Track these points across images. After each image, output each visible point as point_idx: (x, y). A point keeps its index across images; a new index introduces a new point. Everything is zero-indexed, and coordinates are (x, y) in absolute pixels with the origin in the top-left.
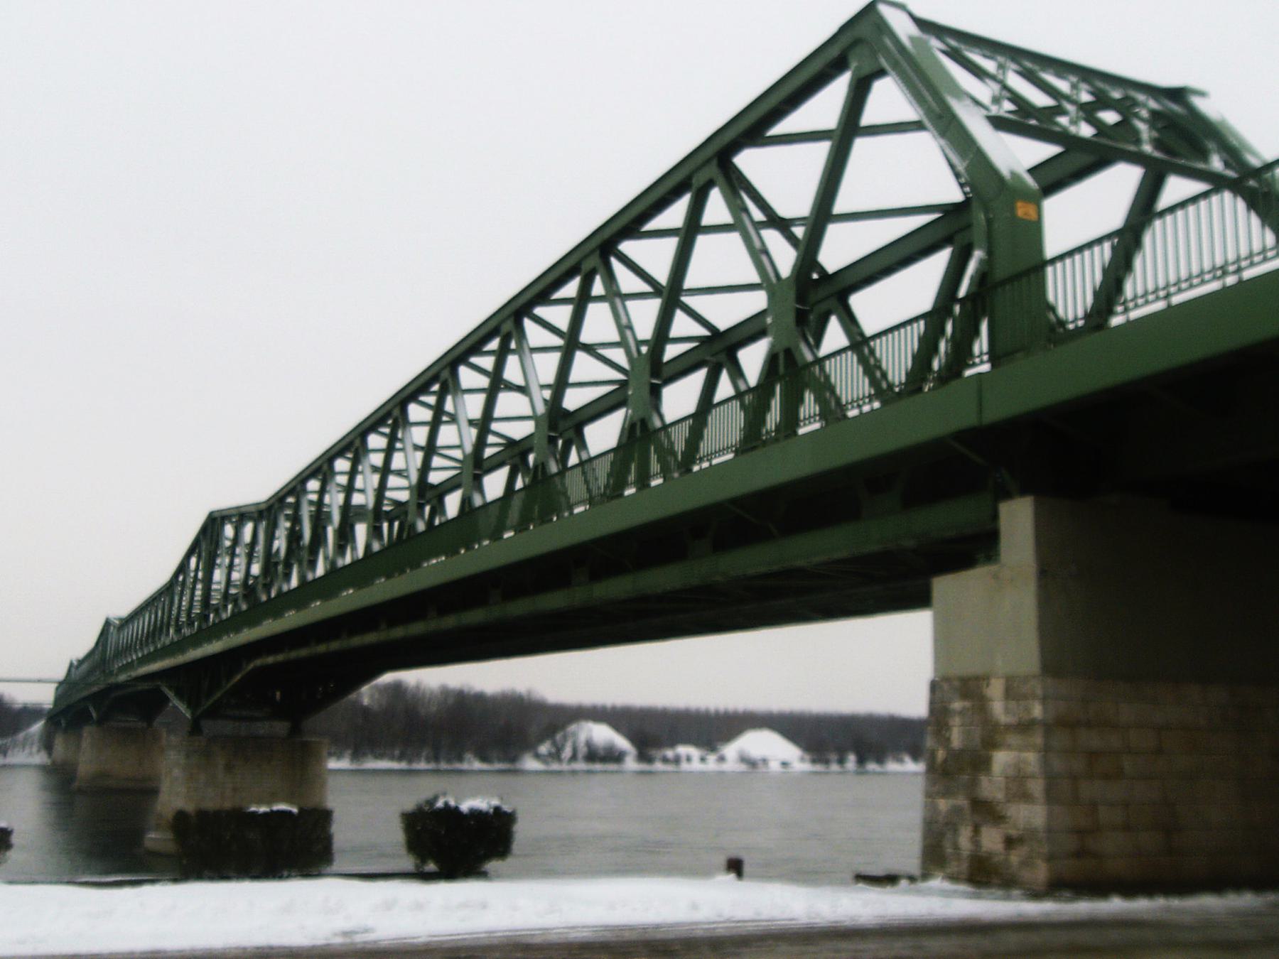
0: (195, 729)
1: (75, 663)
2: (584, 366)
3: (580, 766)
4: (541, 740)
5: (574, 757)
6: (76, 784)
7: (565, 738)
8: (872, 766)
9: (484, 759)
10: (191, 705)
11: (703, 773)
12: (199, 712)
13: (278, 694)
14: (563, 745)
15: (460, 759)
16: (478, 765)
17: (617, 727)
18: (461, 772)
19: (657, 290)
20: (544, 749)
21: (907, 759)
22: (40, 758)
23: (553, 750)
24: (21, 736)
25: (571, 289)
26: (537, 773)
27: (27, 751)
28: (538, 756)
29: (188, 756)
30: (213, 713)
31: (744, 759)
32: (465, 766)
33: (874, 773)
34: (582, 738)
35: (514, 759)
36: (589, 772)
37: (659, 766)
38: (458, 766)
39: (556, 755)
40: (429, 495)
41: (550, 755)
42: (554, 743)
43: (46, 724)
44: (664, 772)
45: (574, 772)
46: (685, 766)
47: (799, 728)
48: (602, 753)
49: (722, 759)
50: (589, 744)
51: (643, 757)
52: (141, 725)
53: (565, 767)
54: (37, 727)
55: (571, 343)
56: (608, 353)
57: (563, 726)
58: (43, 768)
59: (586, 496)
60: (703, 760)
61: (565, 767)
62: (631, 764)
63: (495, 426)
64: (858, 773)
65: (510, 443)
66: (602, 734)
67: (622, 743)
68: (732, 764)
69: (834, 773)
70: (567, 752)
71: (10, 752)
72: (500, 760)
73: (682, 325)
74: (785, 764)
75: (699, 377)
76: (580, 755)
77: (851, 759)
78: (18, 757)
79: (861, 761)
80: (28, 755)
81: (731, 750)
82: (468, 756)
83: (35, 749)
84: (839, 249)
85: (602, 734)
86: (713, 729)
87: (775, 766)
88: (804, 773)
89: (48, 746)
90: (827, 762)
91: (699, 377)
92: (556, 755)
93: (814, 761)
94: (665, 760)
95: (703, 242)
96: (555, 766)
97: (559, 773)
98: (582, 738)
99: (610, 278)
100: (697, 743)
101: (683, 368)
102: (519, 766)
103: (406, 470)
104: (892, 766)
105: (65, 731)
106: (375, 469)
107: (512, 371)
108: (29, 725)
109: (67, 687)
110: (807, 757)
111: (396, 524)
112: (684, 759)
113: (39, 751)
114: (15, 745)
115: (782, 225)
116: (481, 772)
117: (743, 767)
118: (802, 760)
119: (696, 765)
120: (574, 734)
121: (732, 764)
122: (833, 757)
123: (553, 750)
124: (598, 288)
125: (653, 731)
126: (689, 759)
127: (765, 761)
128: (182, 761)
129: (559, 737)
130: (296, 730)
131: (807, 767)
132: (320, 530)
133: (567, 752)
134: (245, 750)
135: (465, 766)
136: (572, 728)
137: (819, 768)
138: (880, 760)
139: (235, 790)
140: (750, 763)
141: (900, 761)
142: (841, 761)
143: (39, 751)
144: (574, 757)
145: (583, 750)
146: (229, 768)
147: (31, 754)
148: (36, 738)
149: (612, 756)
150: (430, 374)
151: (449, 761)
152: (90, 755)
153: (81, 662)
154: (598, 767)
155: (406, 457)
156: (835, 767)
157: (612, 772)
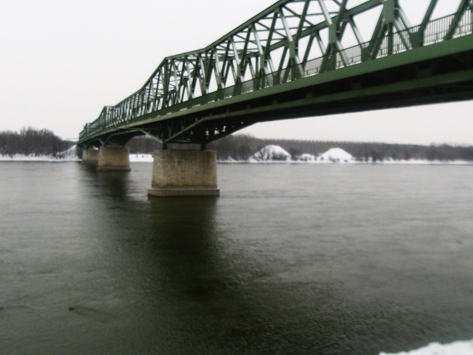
0: (165, 147)
1: (89, 124)
2: (275, 36)
3: (270, 161)
4: (256, 151)
5: (268, 158)
6: (98, 168)
7: (265, 151)
8: (378, 162)
9: (235, 159)
10: (104, 142)
12: (167, 140)
13: (207, 132)
14: (264, 154)
15: (227, 159)
16: (233, 161)
17: (285, 148)
20: (257, 155)
22: (76, 159)
23: (260, 155)
24: (68, 151)
27: (71, 156)
28: (255, 158)
29: (163, 158)
30: (173, 141)
31: (331, 159)
32: (228, 161)
34: (271, 151)
35: (246, 159)
37: (299, 161)
38: (226, 161)
39: (261, 157)
40: (246, 56)
42: (261, 153)
44: (301, 164)
45: (268, 164)
46: (309, 161)
47: (351, 148)
48: (278, 157)
49: (322, 159)
50: (274, 153)
51: (293, 158)
53: (265, 162)
54: (74, 147)
55: (272, 30)
56: (291, 14)
57: (264, 147)
58: (79, 162)
59: (356, 43)
61: (265, 162)
62: (289, 160)
63: (307, 18)
65: (312, 26)
66: (278, 150)
67: (286, 153)
68: (326, 161)
70: (265, 156)
71: (65, 157)
72: (241, 159)
74: (346, 161)
76: (270, 157)
77: (371, 159)
78: (68, 158)
79: (374, 160)
82: (230, 158)
83: (74, 155)
85: (278, 150)
86: (318, 148)
87: (342, 162)
88: (353, 164)
89: (80, 154)
90: (361, 160)
92: (261, 157)
93: (357, 160)
94: (302, 159)
102: (248, 161)
103: (256, 40)
104: (385, 162)
105: (87, 149)
109: (83, 134)
110: (354, 158)
112: (308, 158)
114: (67, 154)
116: (235, 163)
117: (330, 162)
118: (352, 159)
119: (313, 161)
120: (268, 150)
121: (326, 161)
122: (364, 158)
123: (260, 155)
125: (296, 149)
127: (338, 160)
128: (161, 160)
129: (262, 150)
130: (203, 148)
131: (354, 162)
132: (197, 71)
133: (265, 156)
134: (185, 156)
135: (228, 161)
136: (267, 147)
137: (358, 162)
138: (381, 159)
139: (182, 171)
140: (333, 160)
141: (388, 160)
142: (367, 160)
144: (268, 158)
145: (271, 156)
146: (179, 163)
148: (74, 152)
149: (282, 158)
151: (222, 160)
153: (91, 124)
154: (277, 162)
156: (364, 162)
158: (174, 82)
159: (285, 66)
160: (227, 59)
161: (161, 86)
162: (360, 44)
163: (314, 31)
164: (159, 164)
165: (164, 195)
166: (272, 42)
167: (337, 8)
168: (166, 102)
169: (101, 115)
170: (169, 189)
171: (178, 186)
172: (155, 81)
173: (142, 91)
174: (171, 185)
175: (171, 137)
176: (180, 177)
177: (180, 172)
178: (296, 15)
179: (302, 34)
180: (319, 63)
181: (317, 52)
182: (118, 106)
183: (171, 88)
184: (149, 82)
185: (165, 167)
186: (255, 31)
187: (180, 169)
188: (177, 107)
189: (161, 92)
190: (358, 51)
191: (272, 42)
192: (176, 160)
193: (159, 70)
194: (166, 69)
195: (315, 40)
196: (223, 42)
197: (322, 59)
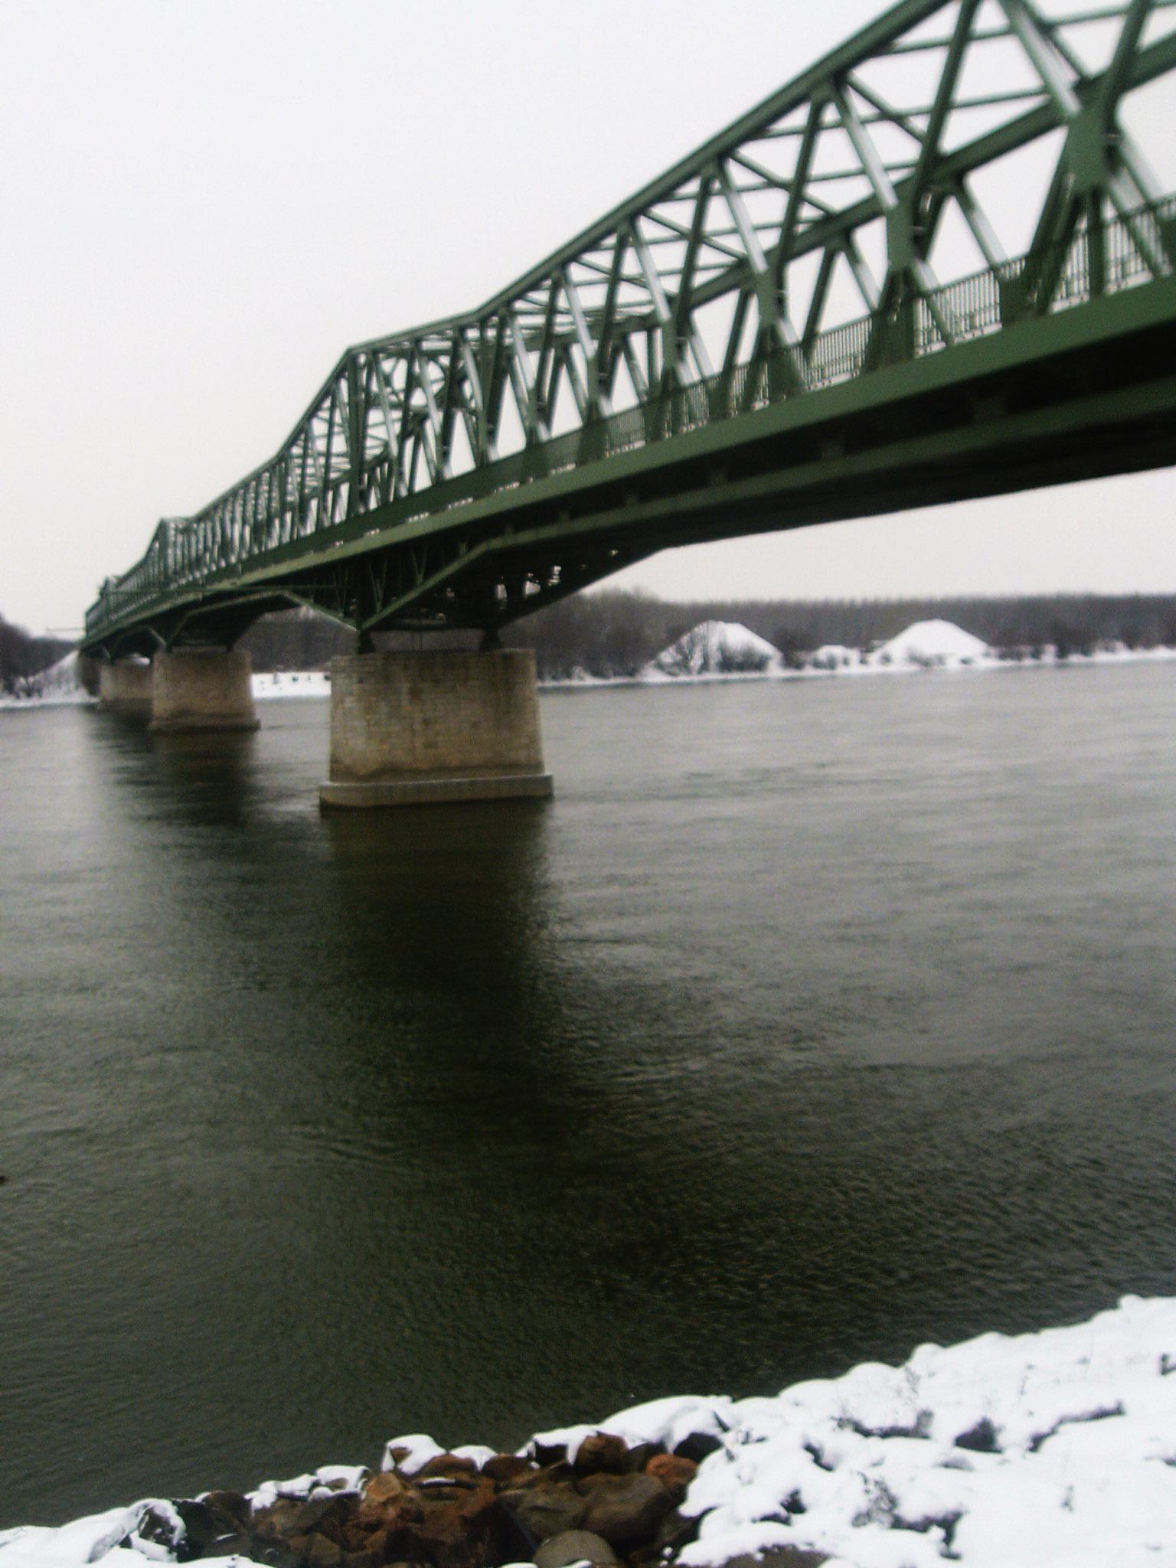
3: (713, 676)
4: (663, 647)
5: (705, 667)
7: (693, 643)
8: (1075, 658)
9: (597, 673)
11: (864, 679)
12: (371, 621)
14: (691, 650)
16: (590, 681)
18: (569, 691)
19: (682, 235)
20: (668, 656)
21: (1119, 645)
22: (81, 696)
23: (679, 657)
24: (54, 671)
25: (799, 117)
26: (663, 686)
27: (64, 688)
28: (661, 667)
29: (361, 681)
31: (914, 659)
32: (575, 683)
33: (1079, 666)
34: (714, 642)
36: (725, 682)
37: (809, 672)
38: (566, 683)
39: (683, 665)
41: (676, 664)
42: (680, 650)
43: (80, 656)
46: (841, 670)
47: (971, 615)
48: (739, 659)
49: (886, 659)
50: (723, 649)
51: (790, 662)
52: (222, 649)
53: (695, 678)
54: (70, 660)
55: (696, 237)
57: (689, 628)
58: (90, 708)
60: (863, 662)
61: (695, 678)
62: (776, 670)
64: (1060, 667)
66: (737, 636)
67: (763, 647)
69: (1027, 668)
70: (696, 661)
71: (45, 691)
72: (616, 674)
73: (807, 212)
75: (731, 300)
78: (55, 696)
79: (1062, 653)
80: (63, 691)
81: (898, 647)
82: (578, 670)
83: (72, 685)
84: (958, 133)
85: (737, 636)
86: (869, 624)
87: (953, 665)
89: (89, 681)
90: (1019, 656)
91: (731, 300)
92: (683, 665)
93: (1002, 657)
94: (817, 665)
95: (975, 54)
96: (683, 678)
97: (689, 685)
98: (714, 642)
99: (844, 108)
100: (848, 643)
101: (713, 292)
102: (638, 679)
104: (1101, 657)
106: (298, 457)
107: (630, 265)
108: (61, 656)
110: (993, 651)
111: (386, 466)
113: (77, 687)
115: (899, 120)
116: (594, 688)
117: (914, 668)
118: (987, 655)
119: (855, 669)
120: (704, 638)
123: (679, 657)
124: (830, 114)
125: (797, 631)
126: (846, 662)
127: (940, 660)
128: (355, 687)
129: (685, 639)
130: (490, 642)
131: (994, 663)
133: (696, 661)
134: (433, 670)
135: (575, 683)
136: (700, 629)
137: (1009, 663)
138: (1086, 651)
139: (426, 722)
142: (1036, 654)
143: (77, 687)
144: (705, 667)
145: (715, 657)
146: (415, 694)
147: (68, 692)
148: (71, 672)
149: (752, 663)
150: (542, 271)
151: (554, 678)
152: (164, 690)
154: (735, 676)
155: (744, 240)
156: (1028, 662)
157: (754, 681)
158: (382, 428)
159: (745, 354)
160: (552, 343)
161: (340, 444)
162: (993, 269)
163: (836, 233)
164: (350, 702)
165: (371, 803)
166: (699, 279)
167: (909, 151)
168: (359, 496)
169: (150, 550)
170: (386, 782)
171: (416, 772)
172: (319, 427)
173: (279, 465)
174: (390, 770)
175: (382, 613)
176: (419, 742)
177: (418, 727)
178: (771, 183)
179: (797, 246)
180: (858, 341)
181: (849, 304)
182: (205, 516)
183: (372, 449)
184: (302, 432)
185: (369, 709)
186: (640, 244)
187: (418, 716)
188: (395, 510)
189: (341, 464)
190: (988, 293)
191: (699, 279)
192: (405, 687)
193: (329, 391)
194: (354, 389)
195: (841, 263)
196: (535, 286)
197: (866, 328)
